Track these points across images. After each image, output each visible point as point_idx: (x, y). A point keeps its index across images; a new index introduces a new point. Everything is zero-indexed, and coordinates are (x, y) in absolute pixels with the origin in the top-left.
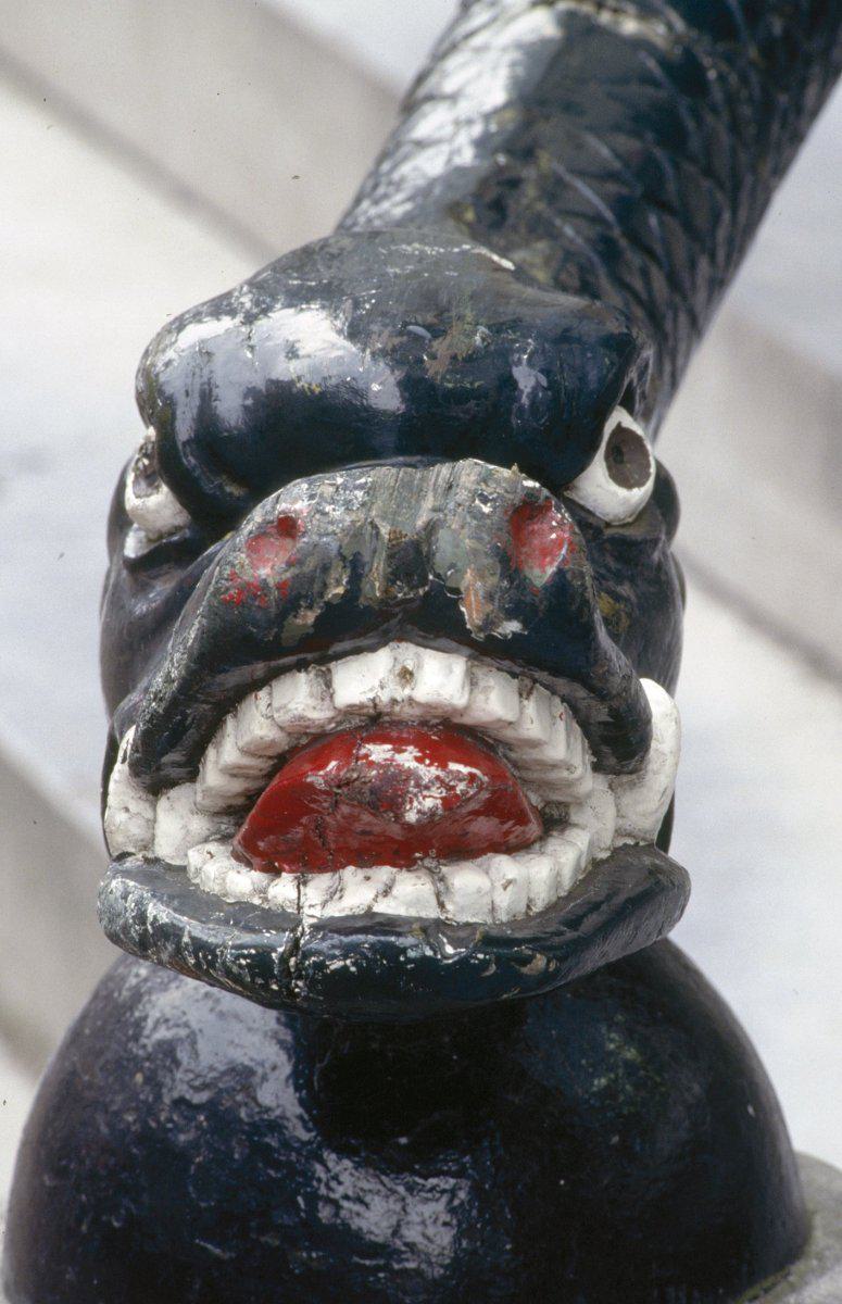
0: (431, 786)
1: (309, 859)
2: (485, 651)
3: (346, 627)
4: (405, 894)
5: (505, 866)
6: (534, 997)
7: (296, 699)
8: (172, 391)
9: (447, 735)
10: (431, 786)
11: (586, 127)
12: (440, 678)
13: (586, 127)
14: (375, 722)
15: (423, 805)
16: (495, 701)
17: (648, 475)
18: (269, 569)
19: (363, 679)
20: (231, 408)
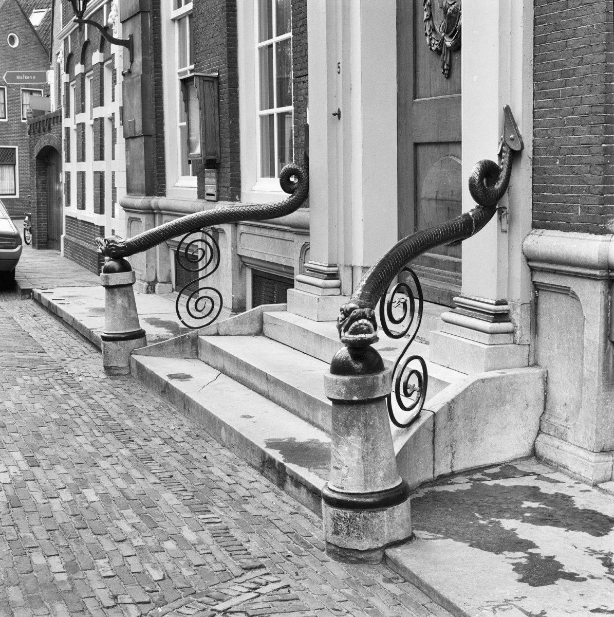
0: (365, 328)
1: (357, 334)
2: (368, 319)
3: (360, 318)
4: (363, 336)
5: (360, 117)
6: (343, 53)
7: (356, 323)
8: (597, 252)
9: (366, 325)
10: (365, 328)
11: (448, 76)
12: (365, 321)
13: (448, 76)
14: (361, 324)
15: (365, 329)
16: (369, 323)
17: (496, 486)
18: (355, 314)
19: (360, 321)
20: (348, 310)
